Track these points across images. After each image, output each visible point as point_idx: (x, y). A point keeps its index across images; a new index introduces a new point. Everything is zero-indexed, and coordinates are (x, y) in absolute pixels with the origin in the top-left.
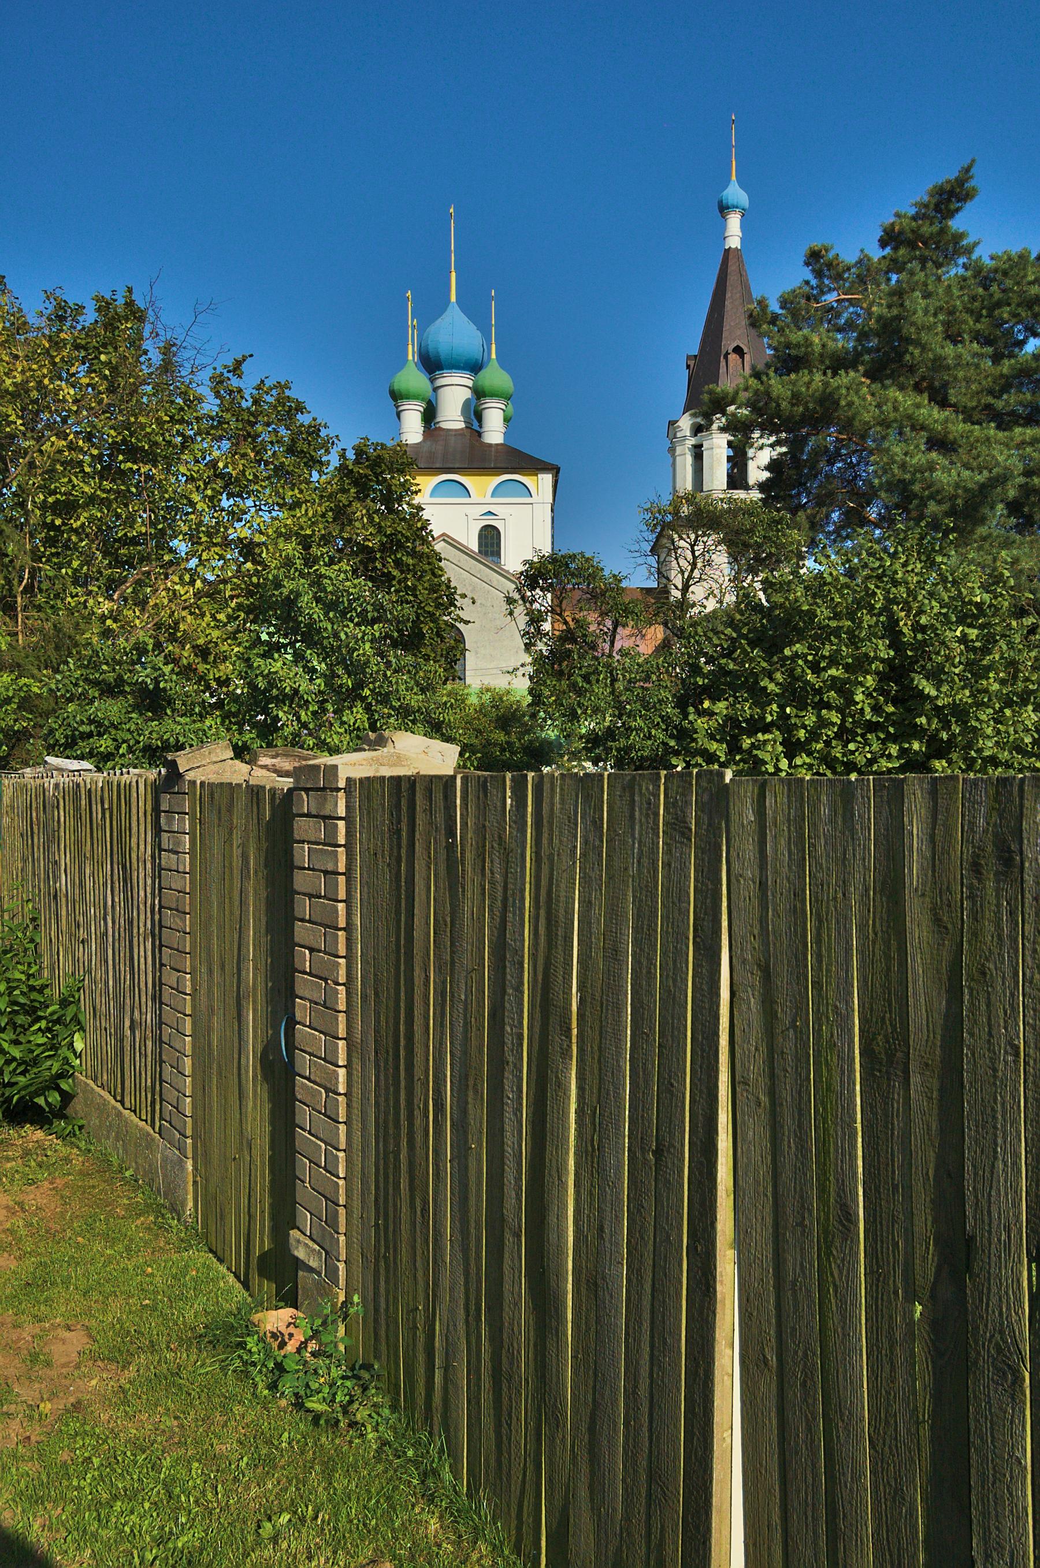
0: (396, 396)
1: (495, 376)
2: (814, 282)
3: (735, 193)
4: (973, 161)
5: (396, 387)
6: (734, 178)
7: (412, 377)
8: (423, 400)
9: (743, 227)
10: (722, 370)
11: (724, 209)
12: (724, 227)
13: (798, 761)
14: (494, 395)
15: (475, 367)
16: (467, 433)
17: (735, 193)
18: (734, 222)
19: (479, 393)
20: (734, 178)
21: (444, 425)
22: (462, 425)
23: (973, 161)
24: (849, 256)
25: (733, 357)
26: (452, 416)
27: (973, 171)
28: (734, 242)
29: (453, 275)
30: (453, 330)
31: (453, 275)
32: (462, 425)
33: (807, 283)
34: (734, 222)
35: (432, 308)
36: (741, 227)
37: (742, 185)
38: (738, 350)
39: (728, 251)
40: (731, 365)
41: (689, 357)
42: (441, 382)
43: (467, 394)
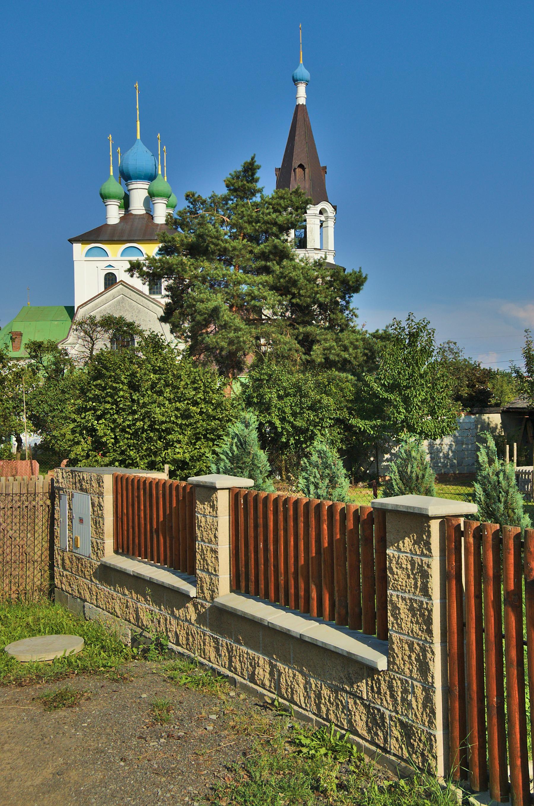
0: (104, 197)
1: (162, 183)
2: (191, 206)
3: (302, 71)
4: (255, 155)
5: (102, 192)
6: (301, 62)
7: (114, 186)
8: (119, 199)
9: (307, 92)
10: (292, 178)
11: (296, 81)
12: (296, 92)
13: (100, 422)
14: (159, 195)
15: (151, 178)
16: (146, 217)
17: (302, 71)
18: (302, 89)
19: (152, 195)
20: (301, 62)
21: (134, 212)
22: (144, 212)
23: (255, 155)
24: (206, 195)
25: (299, 170)
26: (138, 207)
27: (255, 159)
28: (302, 101)
29: (138, 123)
30: (139, 157)
31: (138, 123)
32: (144, 212)
33: (189, 207)
34: (302, 89)
35: (127, 142)
36: (306, 92)
37: (306, 68)
38: (301, 166)
39: (298, 106)
40: (297, 175)
41: (276, 169)
42: (131, 187)
43: (145, 194)
